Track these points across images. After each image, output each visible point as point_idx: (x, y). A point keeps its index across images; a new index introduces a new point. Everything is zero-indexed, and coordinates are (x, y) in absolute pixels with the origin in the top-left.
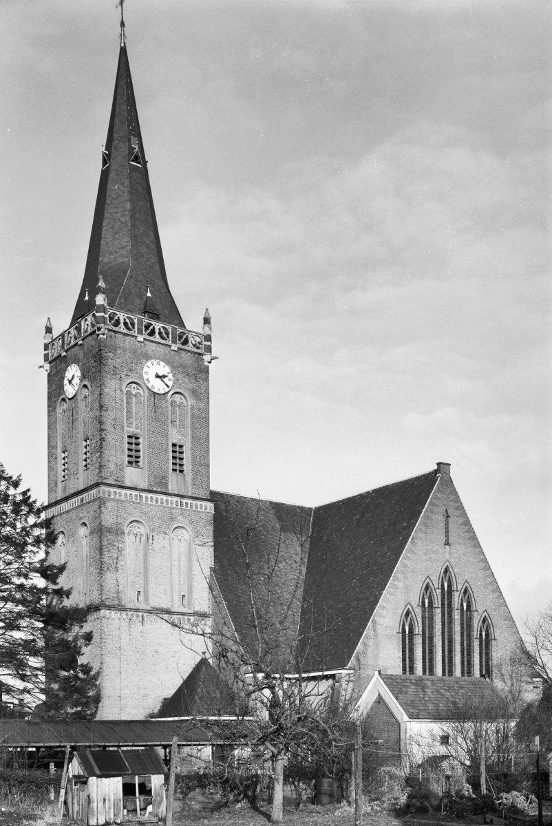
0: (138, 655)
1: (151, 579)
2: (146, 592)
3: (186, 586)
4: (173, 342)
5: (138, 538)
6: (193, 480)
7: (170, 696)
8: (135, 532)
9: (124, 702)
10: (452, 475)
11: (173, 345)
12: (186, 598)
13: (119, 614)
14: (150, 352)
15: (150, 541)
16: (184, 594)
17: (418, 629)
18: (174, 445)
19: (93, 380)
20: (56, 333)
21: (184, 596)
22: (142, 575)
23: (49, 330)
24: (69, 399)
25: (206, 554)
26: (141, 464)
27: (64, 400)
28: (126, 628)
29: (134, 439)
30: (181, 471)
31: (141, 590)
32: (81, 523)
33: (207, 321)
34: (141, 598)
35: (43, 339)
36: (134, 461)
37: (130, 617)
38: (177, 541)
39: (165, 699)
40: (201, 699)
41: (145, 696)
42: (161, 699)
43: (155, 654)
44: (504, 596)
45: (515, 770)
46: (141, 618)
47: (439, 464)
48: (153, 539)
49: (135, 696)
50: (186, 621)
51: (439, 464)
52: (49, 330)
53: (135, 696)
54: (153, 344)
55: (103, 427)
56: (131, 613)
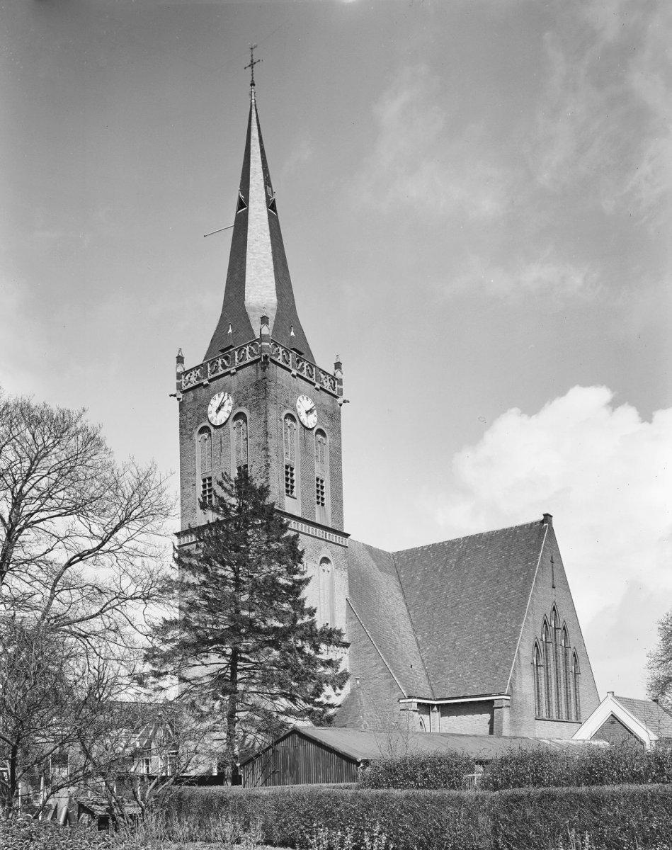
3: (328, 615)
4: (316, 381)
6: (333, 513)
10: (553, 526)
11: (317, 383)
14: (301, 388)
18: (318, 479)
19: (255, 406)
20: (188, 365)
23: (180, 360)
24: (216, 427)
26: (294, 494)
27: (204, 430)
29: (289, 469)
30: (323, 505)
32: (320, 558)
33: (338, 366)
35: (173, 369)
36: (289, 490)
44: (580, 625)
47: (544, 515)
51: (544, 515)
52: (180, 360)
54: (302, 381)
55: (269, 454)
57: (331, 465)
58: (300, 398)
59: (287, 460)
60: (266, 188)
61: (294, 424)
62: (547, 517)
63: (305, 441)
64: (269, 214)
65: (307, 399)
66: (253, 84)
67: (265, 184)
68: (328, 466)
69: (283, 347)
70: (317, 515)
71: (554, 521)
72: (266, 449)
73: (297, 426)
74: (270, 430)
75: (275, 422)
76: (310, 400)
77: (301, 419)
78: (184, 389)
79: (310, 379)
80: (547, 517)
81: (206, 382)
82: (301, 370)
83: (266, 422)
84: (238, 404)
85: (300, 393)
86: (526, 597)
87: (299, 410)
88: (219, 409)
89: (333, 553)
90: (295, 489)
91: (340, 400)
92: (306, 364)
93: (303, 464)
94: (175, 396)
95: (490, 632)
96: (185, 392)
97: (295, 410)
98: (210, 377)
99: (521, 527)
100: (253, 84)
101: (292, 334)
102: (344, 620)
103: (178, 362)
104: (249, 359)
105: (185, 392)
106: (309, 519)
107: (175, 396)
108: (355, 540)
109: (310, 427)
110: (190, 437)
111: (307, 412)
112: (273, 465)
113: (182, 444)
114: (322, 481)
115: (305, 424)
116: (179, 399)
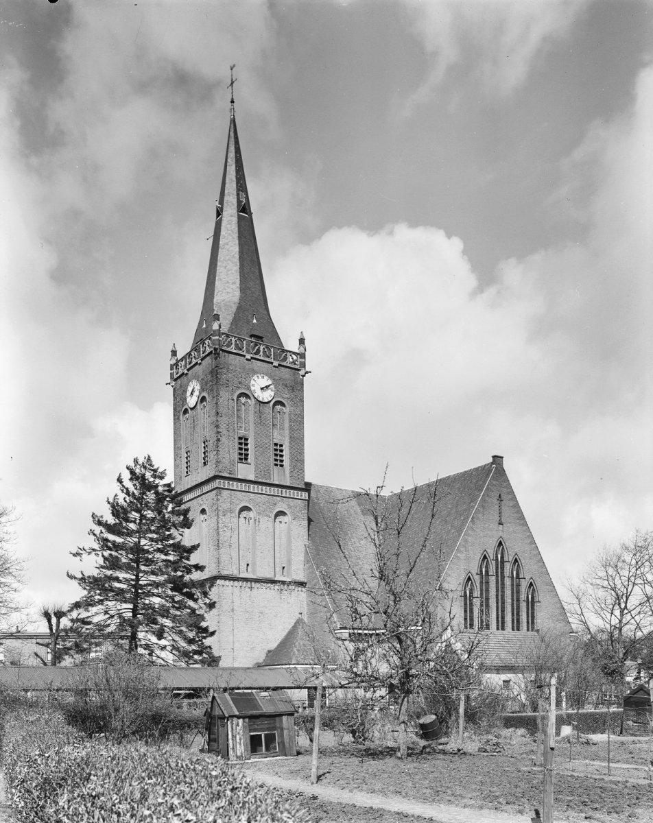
1: (258, 553)
2: (254, 564)
6: (291, 472)
14: (256, 368)
15: (257, 523)
20: (179, 356)
23: (174, 353)
26: (249, 461)
29: (243, 441)
30: (282, 466)
31: (250, 562)
33: (302, 341)
36: (244, 458)
39: (269, 651)
40: (298, 650)
41: (253, 648)
42: (266, 651)
52: (174, 353)
57: (291, 430)
58: (255, 377)
59: (242, 432)
60: (238, 195)
61: (249, 401)
62: (497, 459)
63: (260, 414)
64: (240, 218)
65: (263, 377)
66: (232, 102)
67: (238, 190)
68: (287, 432)
69: (235, 337)
70: (276, 478)
71: (507, 465)
72: (217, 427)
73: (252, 402)
74: (221, 410)
75: (226, 403)
76: (266, 378)
77: (256, 395)
78: (175, 377)
79: (267, 359)
80: (497, 459)
81: (186, 372)
82: (258, 352)
83: (217, 403)
84: (202, 390)
85: (255, 372)
86: (460, 535)
87: (252, 388)
88: (192, 394)
89: (289, 507)
90: (249, 457)
91: (302, 372)
92: (262, 347)
93: (257, 434)
94: (169, 384)
95: (427, 569)
96: (176, 380)
97: (249, 388)
98: (188, 367)
99: (476, 469)
100: (232, 102)
101: (255, 321)
102: (302, 563)
103: (172, 355)
104: (208, 350)
105: (176, 380)
106: (266, 481)
107: (169, 384)
108: (343, 488)
109: (266, 400)
110: (178, 419)
111: (262, 389)
112: (223, 439)
113: (175, 424)
114: (281, 446)
115: (261, 399)
116: (173, 386)
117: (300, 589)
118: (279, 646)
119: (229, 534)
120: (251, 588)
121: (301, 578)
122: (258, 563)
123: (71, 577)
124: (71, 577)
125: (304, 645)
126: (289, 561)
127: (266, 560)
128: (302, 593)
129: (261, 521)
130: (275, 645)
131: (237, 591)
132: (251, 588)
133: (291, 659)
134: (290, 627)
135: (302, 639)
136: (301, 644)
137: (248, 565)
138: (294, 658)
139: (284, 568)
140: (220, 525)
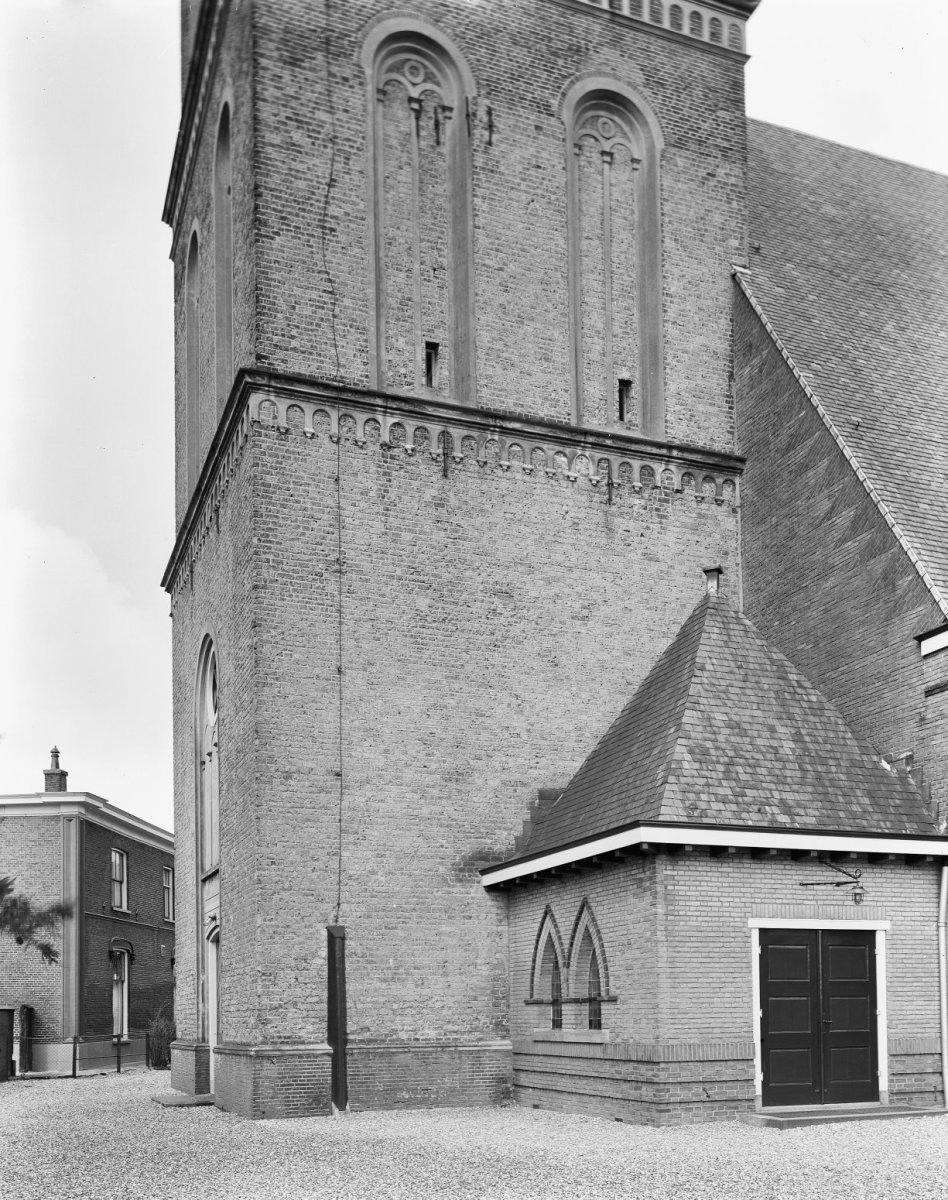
0: (423, 603)
1: (485, 288)
2: (464, 344)
3: (632, 344)
5: (428, 123)
7: (562, 783)
8: (415, 93)
9: (356, 798)
12: (635, 391)
13: (334, 415)
15: (480, 133)
16: (625, 375)
17: (186, 531)
21: (625, 385)
22: (447, 276)
25: (718, 219)
28: (372, 483)
31: (440, 336)
34: (443, 371)
37: (386, 437)
38: (596, 158)
39: (545, 796)
40: (700, 755)
41: (458, 776)
42: (528, 794)
43: (497, 602)
45: (247, 383)
46: (436, 449)
48: (490, 127)
49: (409, 775)
50: (636, 474)
53: (409, 775)
56: (392, 420)
117: (708, 489)
118: (593, 761)
119: (318, 165)
120: (446, 464)
121: (715, 433)
122: (484, 338)
123: (55, 754)
124: (55, 754)
125: (734, 726)
126: (652, 354)
127: (529, 328)
128: (721, 512)
129: (498, 123)
130: (576, 765)
131: (363, 472)
132: (446, 464)
133: (655, 799)
134: (664, 645)
135: (721, 695)
136: (719, 718)
137: (432, 348)
138: (671, 791)
139: (625, 385)
140: (266, 112)
